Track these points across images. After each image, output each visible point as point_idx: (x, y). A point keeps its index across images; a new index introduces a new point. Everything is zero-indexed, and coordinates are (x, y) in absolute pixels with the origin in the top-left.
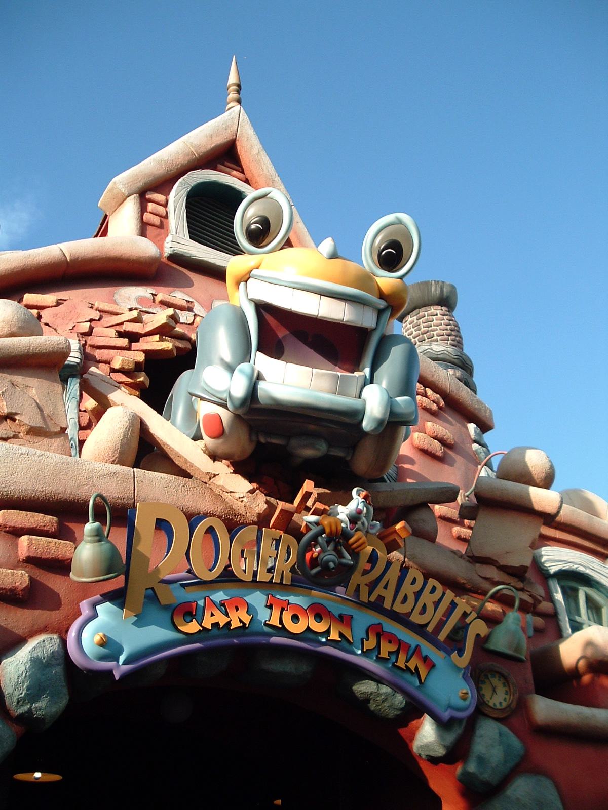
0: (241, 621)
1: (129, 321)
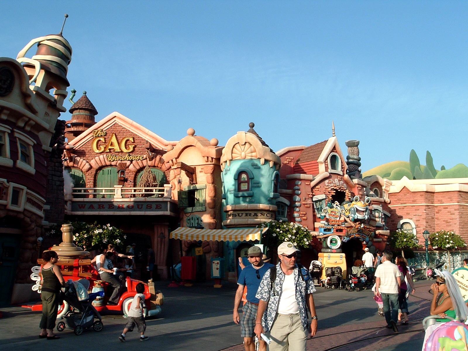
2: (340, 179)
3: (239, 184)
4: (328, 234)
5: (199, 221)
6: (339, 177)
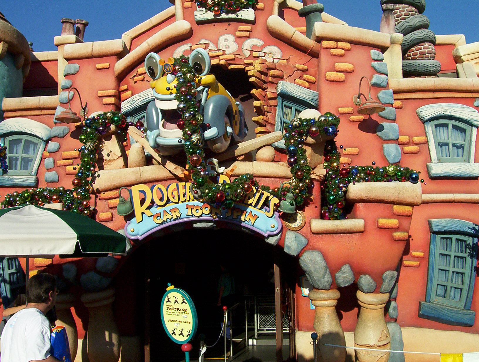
0: (177, 216)
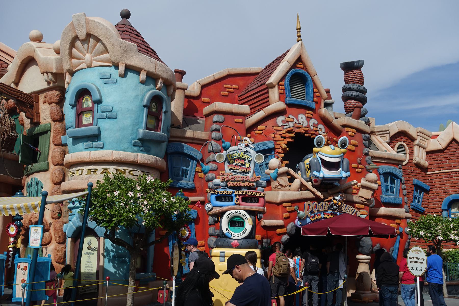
1: (37, 189)
2: (311, 116)
3: (79, 115)
4: (225, 206)
5: (39, 188)
6: (307, 112)
